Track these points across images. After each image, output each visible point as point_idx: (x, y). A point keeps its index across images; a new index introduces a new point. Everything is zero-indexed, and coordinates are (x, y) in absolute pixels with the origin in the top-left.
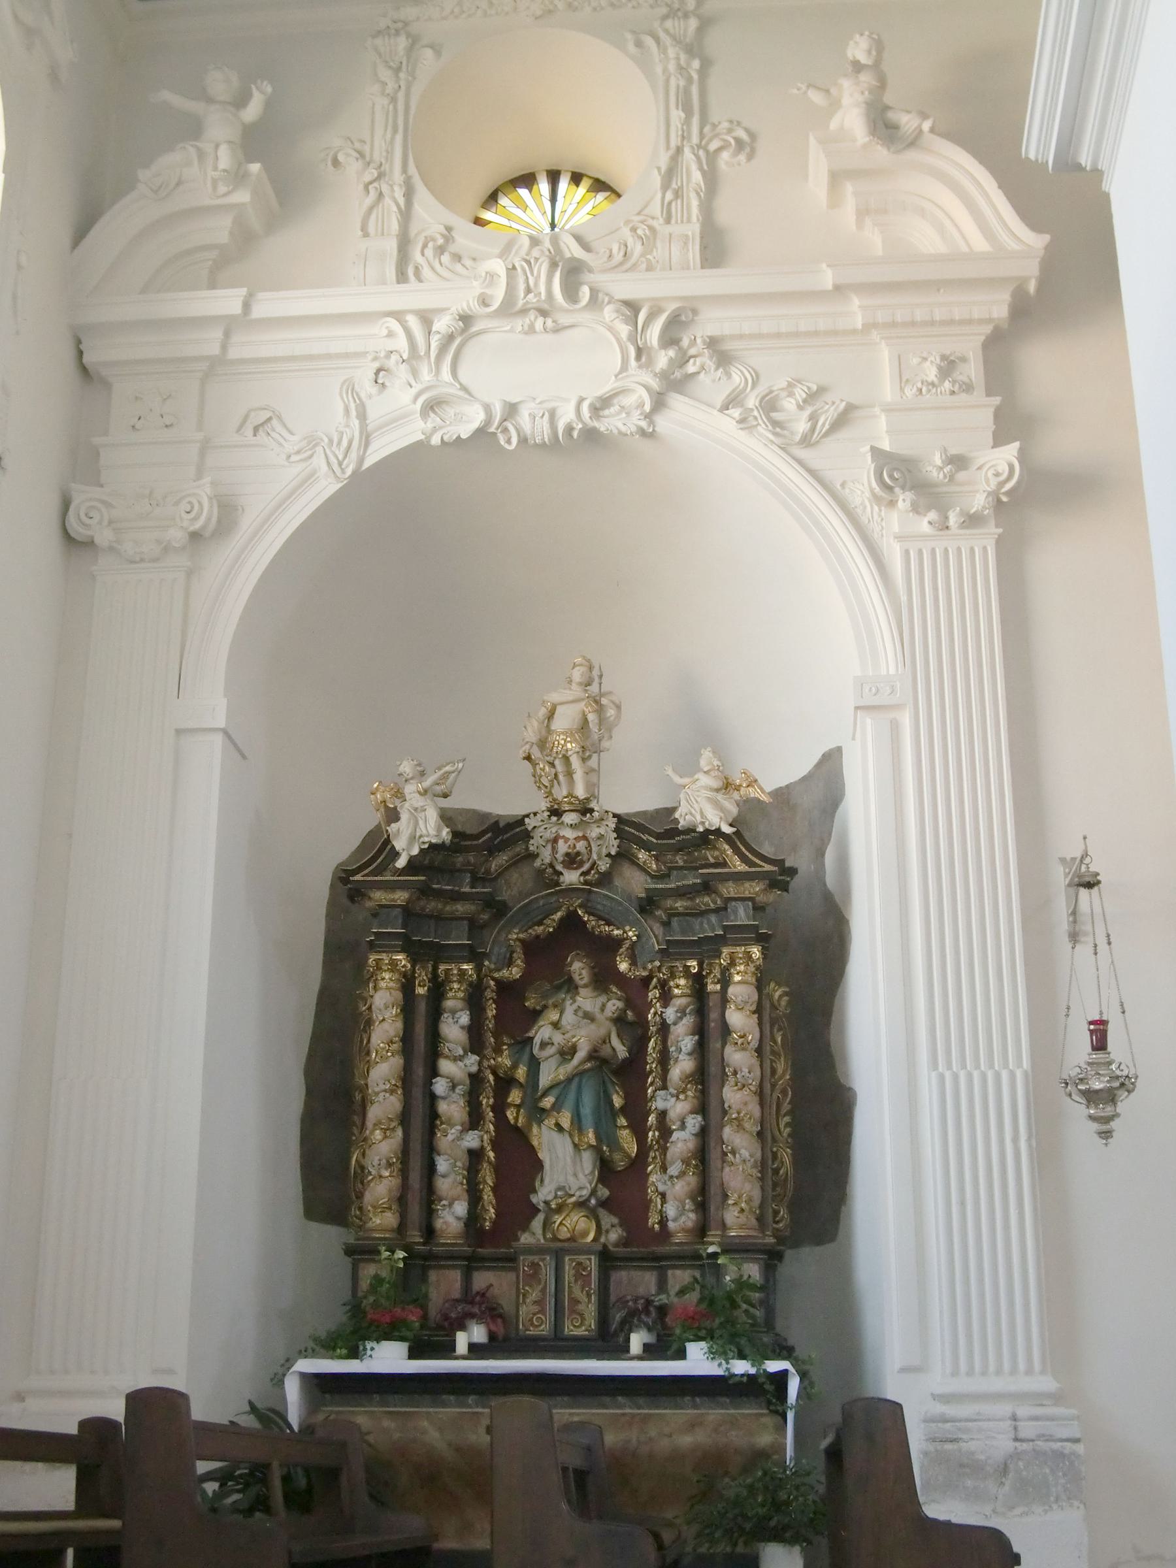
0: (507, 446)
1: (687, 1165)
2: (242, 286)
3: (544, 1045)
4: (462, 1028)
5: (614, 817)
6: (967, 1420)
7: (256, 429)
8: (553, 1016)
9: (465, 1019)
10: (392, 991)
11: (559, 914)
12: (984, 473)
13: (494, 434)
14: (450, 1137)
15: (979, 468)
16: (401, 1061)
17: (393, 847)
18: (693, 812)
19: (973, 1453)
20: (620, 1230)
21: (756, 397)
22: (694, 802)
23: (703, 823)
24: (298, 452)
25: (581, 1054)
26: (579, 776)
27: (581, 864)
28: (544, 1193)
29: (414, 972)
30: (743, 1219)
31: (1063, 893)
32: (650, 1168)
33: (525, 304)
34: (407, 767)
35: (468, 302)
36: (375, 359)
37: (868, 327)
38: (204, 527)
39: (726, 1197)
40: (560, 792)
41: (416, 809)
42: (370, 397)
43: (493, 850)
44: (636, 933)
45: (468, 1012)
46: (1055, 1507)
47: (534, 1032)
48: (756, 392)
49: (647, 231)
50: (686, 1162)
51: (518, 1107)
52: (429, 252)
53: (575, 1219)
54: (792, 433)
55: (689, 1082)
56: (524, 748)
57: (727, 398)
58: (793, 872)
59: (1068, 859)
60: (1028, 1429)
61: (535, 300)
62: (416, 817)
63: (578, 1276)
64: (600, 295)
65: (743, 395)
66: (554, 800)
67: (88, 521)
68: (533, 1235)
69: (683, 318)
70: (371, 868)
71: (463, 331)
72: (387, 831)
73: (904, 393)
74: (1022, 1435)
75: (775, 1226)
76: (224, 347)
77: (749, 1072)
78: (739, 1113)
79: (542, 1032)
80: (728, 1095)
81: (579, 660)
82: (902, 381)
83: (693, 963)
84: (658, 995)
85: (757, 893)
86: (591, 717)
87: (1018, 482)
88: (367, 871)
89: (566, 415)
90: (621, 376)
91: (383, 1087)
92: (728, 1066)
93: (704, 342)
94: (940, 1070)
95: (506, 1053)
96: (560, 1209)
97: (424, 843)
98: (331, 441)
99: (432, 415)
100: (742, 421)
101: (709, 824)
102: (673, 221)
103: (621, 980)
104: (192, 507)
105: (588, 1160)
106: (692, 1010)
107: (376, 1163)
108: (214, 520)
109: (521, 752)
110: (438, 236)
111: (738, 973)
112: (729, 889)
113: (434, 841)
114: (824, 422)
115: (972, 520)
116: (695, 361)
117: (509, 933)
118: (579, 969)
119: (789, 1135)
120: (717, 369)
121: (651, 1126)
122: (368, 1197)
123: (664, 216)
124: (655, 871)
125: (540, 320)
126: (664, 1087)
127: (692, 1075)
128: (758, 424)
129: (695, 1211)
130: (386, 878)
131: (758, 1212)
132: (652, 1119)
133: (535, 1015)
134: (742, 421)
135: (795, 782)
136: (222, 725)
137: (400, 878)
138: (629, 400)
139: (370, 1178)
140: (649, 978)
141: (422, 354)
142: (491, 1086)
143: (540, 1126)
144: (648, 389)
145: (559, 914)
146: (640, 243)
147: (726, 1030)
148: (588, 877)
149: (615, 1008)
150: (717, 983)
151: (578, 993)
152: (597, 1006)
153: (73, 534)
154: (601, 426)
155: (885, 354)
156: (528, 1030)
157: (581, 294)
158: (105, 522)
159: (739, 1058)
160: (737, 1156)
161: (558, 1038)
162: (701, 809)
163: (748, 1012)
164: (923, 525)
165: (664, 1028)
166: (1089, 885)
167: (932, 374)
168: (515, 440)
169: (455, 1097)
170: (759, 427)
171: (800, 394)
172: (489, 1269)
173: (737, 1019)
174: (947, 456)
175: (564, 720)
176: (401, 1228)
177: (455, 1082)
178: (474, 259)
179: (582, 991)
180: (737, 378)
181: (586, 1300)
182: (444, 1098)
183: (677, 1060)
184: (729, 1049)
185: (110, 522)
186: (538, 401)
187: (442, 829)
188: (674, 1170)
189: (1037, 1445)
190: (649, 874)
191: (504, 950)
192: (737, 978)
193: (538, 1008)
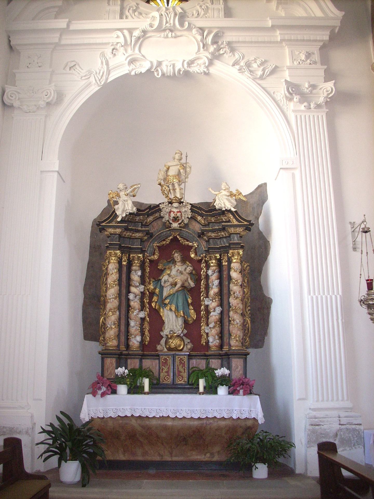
0: (157, 76)
1: (216, 324)
2: (67, 18)
3: (165, 282)
4: (138, 276)
5: (190, 205)
6: (323, 418)
7: (70, 68)
8: (168, 272)
9: (139, 273)
10: (116, 264)
11: (171, 238)
12: (322, 91)
13: (153, 72)
14: (135, 314)
15: (321, 89)
16: (118, 288)
17: (116, 213)
18: (221, 203)
19: (325, 429)
20: (191, 344)
21: (244, 62)
22: (221, 200)
23: (225, 207)
24: (85, 76)
25: (178, 285)
26: (178, 190)
27: (179, 220)
28: (166, 332)
29: (122, 257)
30: (237, 344)
31: (351, 234)
32: (202, 324)
33: (165, 27)
34: (121, 186)
35: (145, 26)
36: (112, 45)
37: (282, 41)
38: (52, 100)
39: (230, 335)
40: (172, 196)
41: (124, 201)
42: (110, 58)
43: (149, 215)
44: (197, 244)
45: (141, 271)
46: (353, 448)
47: (162, 277)
48: (243, 61)
49: (205, 7)
50: (216, 323)
51: (156, 302)
52: (131, 11)
53: (177, 341)
54: (256, 75)
55: (217, 295)
56: (158, 181)
57: (234, 62)
58: (252, 224)
59: (352, 222)
60: (344, 421)
61: (169, 26)
62: (124, 203)
63: (181, 363)
64: (192, 25)
65: (239, 62)
66: (170, 198)
67: (11, 98)
68: (161, 346)
69: (219, 34)
70: (108, 221)
71: (143, 36)
72: (114, 208)
73: (294, 64)
74: (342, 423)
75: (245, 344)
76: (60, 39)
77: (239, 293)
78: (235, 307)
79: (165, 277)
80: (232, 301)
81: (178, 152)
82: (293, 60)
83: (218, 256)
84: (205, 266)
85: (241, 232)
86: (182, 171)
87: (334, 94)
88: (107, 222)
89: (179, 66)
90: (198, 53)
91: (112, 297)
92: (232, 291)
93: (226, 43)
94: (312, 295)
95: (152, 284)
96: (171, 338)
97: (127, 212)
98: (96, 73)
99: (132, 64)
100: (239, 70)
101: (227, 208)
102: (214, 4)
103: (191, 260)
104: (48, 94)
105: (180, 321)
106: (217, 271)
107: (110, 323)
108: (55, 98)
109: (158, 182)
110: (134, 6)
111: (235, 259)
112: (232, 230)
113: (131, 212)
114: (267, 71)
115: (318, 106)
116: (223, 50)
117: (154, 244)
118: (177, 256)
119: (249, 314)
120: (230, 53)
121: (202, 310)
122: (107, 335)
123: (211, 2)
124: (203, 223)
125: (170, 33)
126: (207, 296)
127: (217, 293)
128: (245, 71)
129: (219, 339)
130: (113, 224)
131: (242, 341)
132: (202, 307)
133: (162, 271)
134: (239, 70)
135: (247, 195)
136: (57, 170)
137: (118, 224)
138: (200, 62)
139: (108, 328)
140: (201, 260)
141: (129, 43)
142: (148, 296)
143: (163, 309)
144: (207, 58)
145: (171, 238)
146: (203, 11)
147: (230, 278)
148: (181, 225)
149: (190, 269)
150: (226, 262)
151: (176, 264)
152: (183, 269)
153: (5, 102)
154: (191, 70)
155: (287, 51)
156: (160, 276)
157: (185, 25)
158: (17, 99)
159: (235, 288)
160: (235, 322)
161: (171, 280)
162: (224, 203)
163: (238, 273)
164: (302, 107)
165: (207, 277)
166: (366, 232)
167: (303, 57)
168: (160, 74)
169: (136, 300)
170: (245, 72)
171: (259, 62)
172: (148, 359)
173: (234, 275)
174: (310, 84)
175: (172, 172)
176: (118, 346)
177: (136, 295)
178: (146, 14)
179: (178, 264)
180: (237, 56)
181: (184, 371)
182: (133, 300)
183: (212, 288)
184: (231, 285)
185: (19, 99)
186: (168, 61)
187: (134, 208)
188: (211, 325)
189: (347, 426)
190: (201, 224)
191: (152, 249)
192: (234, 261)
193: (163, 269)
